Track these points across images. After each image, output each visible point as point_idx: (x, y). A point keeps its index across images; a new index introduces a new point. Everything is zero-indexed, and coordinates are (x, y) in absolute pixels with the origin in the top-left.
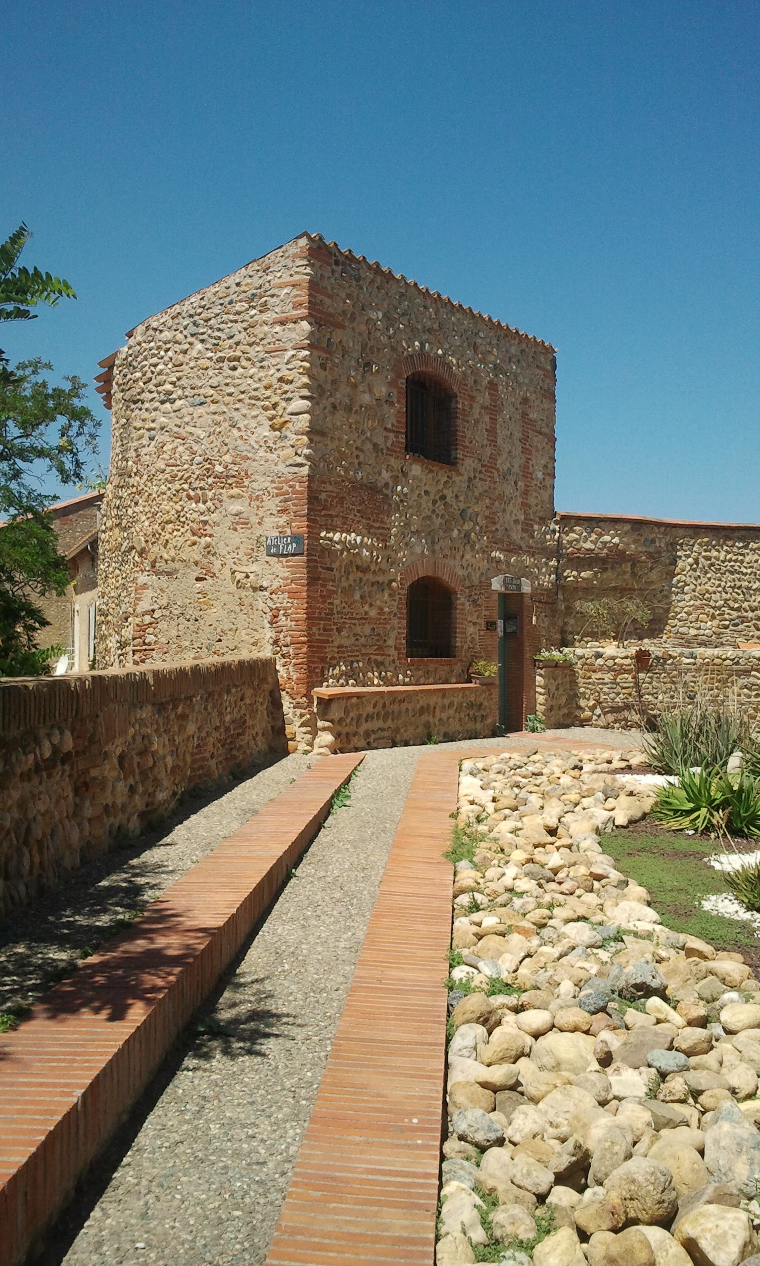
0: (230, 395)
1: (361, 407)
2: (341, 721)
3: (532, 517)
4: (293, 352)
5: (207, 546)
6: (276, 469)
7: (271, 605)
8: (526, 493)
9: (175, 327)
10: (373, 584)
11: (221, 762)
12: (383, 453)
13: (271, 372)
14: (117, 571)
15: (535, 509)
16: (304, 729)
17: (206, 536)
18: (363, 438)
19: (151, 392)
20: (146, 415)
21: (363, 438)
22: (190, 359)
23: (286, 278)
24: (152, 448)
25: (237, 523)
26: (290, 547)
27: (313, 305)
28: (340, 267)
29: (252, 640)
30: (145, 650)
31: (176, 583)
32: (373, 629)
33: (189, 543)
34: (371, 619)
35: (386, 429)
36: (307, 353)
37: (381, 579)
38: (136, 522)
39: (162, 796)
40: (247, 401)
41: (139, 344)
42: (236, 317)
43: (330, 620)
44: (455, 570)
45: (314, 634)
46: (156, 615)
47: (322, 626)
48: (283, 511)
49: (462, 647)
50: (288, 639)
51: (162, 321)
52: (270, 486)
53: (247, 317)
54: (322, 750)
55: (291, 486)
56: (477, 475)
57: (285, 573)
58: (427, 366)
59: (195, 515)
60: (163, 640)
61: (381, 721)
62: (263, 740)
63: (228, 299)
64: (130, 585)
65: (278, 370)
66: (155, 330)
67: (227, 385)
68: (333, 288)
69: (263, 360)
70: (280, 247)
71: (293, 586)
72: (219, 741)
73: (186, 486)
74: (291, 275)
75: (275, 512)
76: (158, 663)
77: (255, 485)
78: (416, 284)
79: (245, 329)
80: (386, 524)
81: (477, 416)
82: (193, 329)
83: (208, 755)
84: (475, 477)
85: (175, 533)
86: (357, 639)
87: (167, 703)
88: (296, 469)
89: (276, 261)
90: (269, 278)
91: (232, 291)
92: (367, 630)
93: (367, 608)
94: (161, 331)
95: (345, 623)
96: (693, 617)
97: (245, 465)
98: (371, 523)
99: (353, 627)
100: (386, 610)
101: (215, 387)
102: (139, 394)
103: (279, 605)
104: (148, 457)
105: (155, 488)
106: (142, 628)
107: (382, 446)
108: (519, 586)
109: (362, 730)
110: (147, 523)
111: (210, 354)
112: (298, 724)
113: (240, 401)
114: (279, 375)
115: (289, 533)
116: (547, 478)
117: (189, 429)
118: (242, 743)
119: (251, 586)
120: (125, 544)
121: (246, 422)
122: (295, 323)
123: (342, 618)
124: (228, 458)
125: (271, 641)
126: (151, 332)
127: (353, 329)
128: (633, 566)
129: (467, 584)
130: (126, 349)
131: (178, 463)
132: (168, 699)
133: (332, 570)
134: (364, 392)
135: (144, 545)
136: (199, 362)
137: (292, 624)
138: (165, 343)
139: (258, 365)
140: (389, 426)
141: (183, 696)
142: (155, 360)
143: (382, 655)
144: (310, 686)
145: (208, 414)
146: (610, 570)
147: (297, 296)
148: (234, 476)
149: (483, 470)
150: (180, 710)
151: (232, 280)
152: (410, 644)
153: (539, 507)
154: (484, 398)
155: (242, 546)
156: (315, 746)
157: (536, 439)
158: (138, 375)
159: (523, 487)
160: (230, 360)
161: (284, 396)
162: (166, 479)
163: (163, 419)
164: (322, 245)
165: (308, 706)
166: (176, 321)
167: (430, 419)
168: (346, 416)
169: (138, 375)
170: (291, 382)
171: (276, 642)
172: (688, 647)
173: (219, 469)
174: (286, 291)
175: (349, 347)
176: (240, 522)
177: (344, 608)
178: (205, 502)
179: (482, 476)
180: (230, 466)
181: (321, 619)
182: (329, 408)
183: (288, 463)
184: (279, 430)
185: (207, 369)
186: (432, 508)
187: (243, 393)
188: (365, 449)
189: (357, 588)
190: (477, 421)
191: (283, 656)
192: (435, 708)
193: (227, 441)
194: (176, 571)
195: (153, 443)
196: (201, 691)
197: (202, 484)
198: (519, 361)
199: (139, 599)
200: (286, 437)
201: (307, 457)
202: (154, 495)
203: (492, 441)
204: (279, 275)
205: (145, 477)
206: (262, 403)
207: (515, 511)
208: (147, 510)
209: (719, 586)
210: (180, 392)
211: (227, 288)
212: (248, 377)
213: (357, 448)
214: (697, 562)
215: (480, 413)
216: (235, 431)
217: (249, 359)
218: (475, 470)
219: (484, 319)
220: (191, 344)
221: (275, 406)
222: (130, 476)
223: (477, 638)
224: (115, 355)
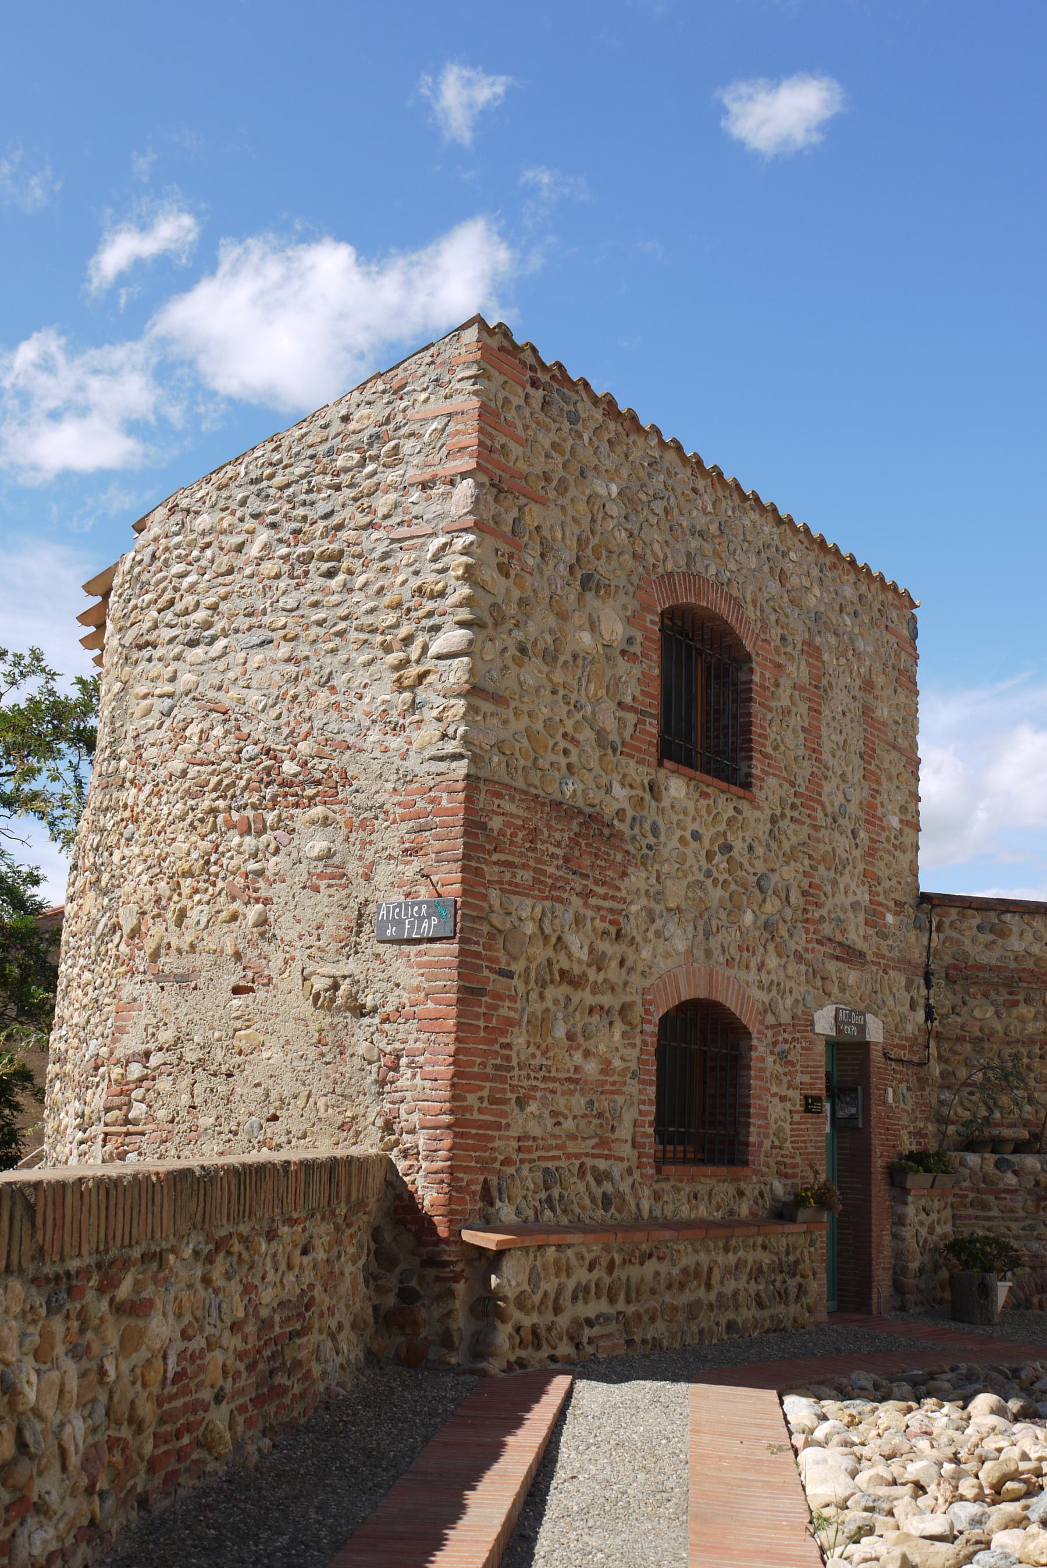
0: (320, 623)
1: (575, 657)
3: (881, 899)
7: (382, 1045)
8: (871, 853)
9: (222, 504)
11: (242, 1409)
12: (614, 750)
15: (887, 884)
18: (578, 716)
21: (578, 716)
25: (320, 876)
26: (425, 925)
27: (485, 450)
28: (541, 392)
30: (128, 1134)
31: (194, 997)
32: (591, 1102)
33: (223, 915)
34: (586, 1082)
35: (620, 704)
36: (470, 538)
37: (606, 1000)
43: (503, 1080)
44: (743, 993)
45: (470, 1109)
46: (153, 1061)
47: (485, 1093)
48: (413, 852)
49: (761, 1145)
50: (415, 1118)
51: (199, 495)
55: (432, 801)
56: (788, 811)
58: (698, 595)
60: (161, 1114)
61: (604, 1300)
62: (354, 1339)
63: (326, 446)
64: (107, 1000)
65: (416, 573)
68: (526, 427)
70: (427, 348)
71: (430, 1005)
72: (240, 1356)
79: (355, 499)
80: (619, 889)
81: (786, 702)
82: (255, 505)
83: (207, 1395)
84: (783, 816)
86: (558, 1124)
87: (83, 1273)
88: (442, 766)
89: (420, 373)
92: (578, 1103)
93: (578, 1057)
95: (534, 1088)
98: (592, 886)
99: (549, 1096)
100: (617, 1063)
101: (292, 610)
103: (398, 1045)
104: (155, 749)
106: (123, 1090)
107: (614, 737)
108: (862, 1028)
109: (563, 1321)
114: (415, 583)
116: (907, 830)
118: (302, 1355)
122: (452, 483)
123: (528, 1077)
125: (380, 1122)
129: (770, 1019)
132: (88, 1260)
133: (510, 975)
134: (581, 628)
140: (628, 700)
141: (136, 1253)
143: (607, 1157)
146: (1022, 1004)
147: (458, 432)
149: (798, 801)
150: (124, 1291)
152: (662, 1136)
153: (894, 881)
154: (798, 671)
155: (329, 922)
157: (887, 758)
159: (867, 842)
160: (324, 557)
166: (225, 493)
167: (704, 697)
168: (546, 669)
170: (442, 594)
173: (289, 768)
175: (554, 539)
177: (533, 1056)
179: (796, 814)
181: (486, 1078)
182: (513, 651)
183: (427, 754)
184: (412, 688)
186: (705, 866)
188: (580, 737)
189: (560, 1016)
190: (786, 712)
196: (196, 1238)
203: (814, 750)
207: (853, 887)
208: (146, 851)
211: (325, 427)
213: (565, 735)
215: (791, 697)
223: (787, 1127)
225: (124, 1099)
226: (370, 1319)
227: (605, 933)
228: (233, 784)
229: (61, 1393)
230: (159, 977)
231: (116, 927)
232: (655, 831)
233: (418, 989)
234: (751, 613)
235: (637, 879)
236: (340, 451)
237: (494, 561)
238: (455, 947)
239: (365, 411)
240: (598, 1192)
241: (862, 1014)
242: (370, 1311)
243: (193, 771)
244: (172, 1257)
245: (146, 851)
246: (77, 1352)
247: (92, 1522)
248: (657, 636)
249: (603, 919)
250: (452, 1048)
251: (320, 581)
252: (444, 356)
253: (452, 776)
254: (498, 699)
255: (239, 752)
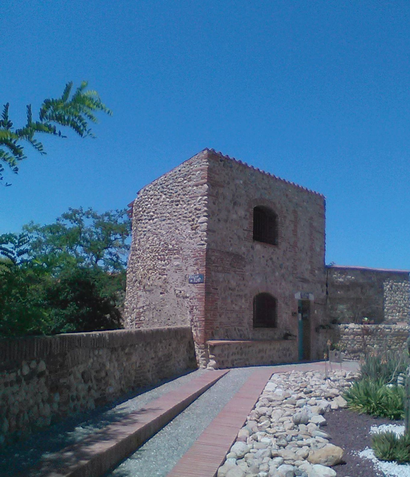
0: (176, 216)
1: (232, 220)
2: (219, 355)
4: (200, 197)
5: (165, 279)
6: (193, 246)
8: (311, 257)
9: (155, 189)
10: (237, 296)
13: (192, 206)
14: (131, 290)
16: (203, 358)
17: (164, 275)
19: (145, 216)
20: (143, 225)
22: (160, 202)
23: (199, 167)
24: (145, 239)
28: (223, 162)
29: (182, 319)
30: (140, 323)
31: (152, 295)
33: (158, 278)
35: (243, 230)
36: (206, 197)
37: (241, 293)
38: (138, 269)
39: (111, 390)
40: (182, 218)
41: (141, 197)
42: (178, 184)
46: (145, 308)
48: (196, 264)
52: (191, 254)
53: (183, 184)
54: (211, 368)
55: (199, 254)
57: (196, 290)
59: (160, 266)
60: (147, 319)
63: (175, 177)
65: (195, 205)
66: (147, 191)
67: (174, 212)
69: (189, 201)
73: (157, 254)
74: (201, 166)
75: (192, 265)
76: (144, 328)
77: (184, 253)
78: (258, 170)
79: (182, 189)
82: (162, 190)
84: (287, 250)
85: (153, 274)
88: (201, 246)
90: (192, 167)
91: (177, 173)
92: (234, 315)
94: (150, 191)
96: (390, 311)
97: (181, 245)
100: (243, 307)
102: (141, 217)
103: (193, 304)
105: (145, 255)
106: (139, 314)
108: (308, 297)
110: (142, 270)
111: (168, 200)
112: (200, 356)
113: (179, 218)
114: (195, 207)
115: (198, 273)
117: (159, 230)
119: (182, 296)
120: (134, 279)
121: (181, 227)
122: (202, 185)
124: (174, 242)
126: (146, 192)
127: (229, 188)
128: (362, 289)
130: (137, 199)
131: (154, 244)
133: (217, 289)
135: (140, 279)
136: (164, 203)
137: (198, 313)
138: (151, 196)
139: (187, 203)
141: (129, 345)
142: (147, 203)
144: (206, 339)
145: (166, 224)
147: (203, 174)
148: (176, 250)
151: (177, 169)
156: (208, 366)
158: (141, 209)
160: (176, 201)
161: (197, 216)
162: (150, 252)
163: (149, 227)
164: (214, 153)
165: (205, 348)
167: (264, 226)
169: (141, 209)
170: (200, 210)
171: (192, 321)
172: (388, 324)
173: (170, 247)
174: (198, 172)
176: (178, 269)
178: (164, 261)
180: (175, 245)
183: (198, 244)
184: (195, 230)
185: (166, 205)
187: (180, 215)
191: (195, 326)
192: (266, 350)
193: (174, 235)
194: (153, 290)
195: (145, 237)
197: (163, 253)
198: (308, 202)
199: (138, 302)
200: (197, 233)
201: (206, 241)
202: (145, 258)
204: (196, 166)
205: (142, 251)
206: (188, 219)
208: (142, 264)
209: (402, 297)
210: (156, 216)
211: (175, 172)
212: (183, 209)
214: (391, 287)
216: (177, 231)
217: (183, 201)
218: (287, 247)
219: (291, 184)
220: (161, 196)
221: (193, 220)
222: (136, 251)
224: (133, 202)
225: (139, 316)
226: (188, 359)
227: (240, 280)
228: (159, 250)
229: (114, 367)
230: (145, 291)
231: (137, 280)
232: (252, 256)
233: (197, 293)
234: (278, 206)
235: (248, 267)
236: (179, 178)
237: (212, 201)
238: (204, 284)
239: (184, 169)
240: (239, 334)
241: (308, 294)
242: (188, 358)
243: (150, 248)
244: (137, 346)
245: (142, 264)
246: (117, 360)
247: (121, 389)
248: (252, 214)
249: (240, 276)
250: (204, 305)
251: (176, 206)
252: (200, 157)
253: (203, 248)
254: (214, 232)
255: (160, 243)
